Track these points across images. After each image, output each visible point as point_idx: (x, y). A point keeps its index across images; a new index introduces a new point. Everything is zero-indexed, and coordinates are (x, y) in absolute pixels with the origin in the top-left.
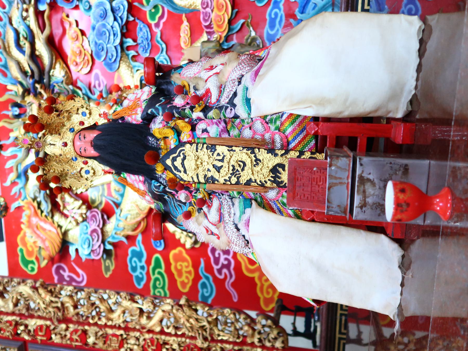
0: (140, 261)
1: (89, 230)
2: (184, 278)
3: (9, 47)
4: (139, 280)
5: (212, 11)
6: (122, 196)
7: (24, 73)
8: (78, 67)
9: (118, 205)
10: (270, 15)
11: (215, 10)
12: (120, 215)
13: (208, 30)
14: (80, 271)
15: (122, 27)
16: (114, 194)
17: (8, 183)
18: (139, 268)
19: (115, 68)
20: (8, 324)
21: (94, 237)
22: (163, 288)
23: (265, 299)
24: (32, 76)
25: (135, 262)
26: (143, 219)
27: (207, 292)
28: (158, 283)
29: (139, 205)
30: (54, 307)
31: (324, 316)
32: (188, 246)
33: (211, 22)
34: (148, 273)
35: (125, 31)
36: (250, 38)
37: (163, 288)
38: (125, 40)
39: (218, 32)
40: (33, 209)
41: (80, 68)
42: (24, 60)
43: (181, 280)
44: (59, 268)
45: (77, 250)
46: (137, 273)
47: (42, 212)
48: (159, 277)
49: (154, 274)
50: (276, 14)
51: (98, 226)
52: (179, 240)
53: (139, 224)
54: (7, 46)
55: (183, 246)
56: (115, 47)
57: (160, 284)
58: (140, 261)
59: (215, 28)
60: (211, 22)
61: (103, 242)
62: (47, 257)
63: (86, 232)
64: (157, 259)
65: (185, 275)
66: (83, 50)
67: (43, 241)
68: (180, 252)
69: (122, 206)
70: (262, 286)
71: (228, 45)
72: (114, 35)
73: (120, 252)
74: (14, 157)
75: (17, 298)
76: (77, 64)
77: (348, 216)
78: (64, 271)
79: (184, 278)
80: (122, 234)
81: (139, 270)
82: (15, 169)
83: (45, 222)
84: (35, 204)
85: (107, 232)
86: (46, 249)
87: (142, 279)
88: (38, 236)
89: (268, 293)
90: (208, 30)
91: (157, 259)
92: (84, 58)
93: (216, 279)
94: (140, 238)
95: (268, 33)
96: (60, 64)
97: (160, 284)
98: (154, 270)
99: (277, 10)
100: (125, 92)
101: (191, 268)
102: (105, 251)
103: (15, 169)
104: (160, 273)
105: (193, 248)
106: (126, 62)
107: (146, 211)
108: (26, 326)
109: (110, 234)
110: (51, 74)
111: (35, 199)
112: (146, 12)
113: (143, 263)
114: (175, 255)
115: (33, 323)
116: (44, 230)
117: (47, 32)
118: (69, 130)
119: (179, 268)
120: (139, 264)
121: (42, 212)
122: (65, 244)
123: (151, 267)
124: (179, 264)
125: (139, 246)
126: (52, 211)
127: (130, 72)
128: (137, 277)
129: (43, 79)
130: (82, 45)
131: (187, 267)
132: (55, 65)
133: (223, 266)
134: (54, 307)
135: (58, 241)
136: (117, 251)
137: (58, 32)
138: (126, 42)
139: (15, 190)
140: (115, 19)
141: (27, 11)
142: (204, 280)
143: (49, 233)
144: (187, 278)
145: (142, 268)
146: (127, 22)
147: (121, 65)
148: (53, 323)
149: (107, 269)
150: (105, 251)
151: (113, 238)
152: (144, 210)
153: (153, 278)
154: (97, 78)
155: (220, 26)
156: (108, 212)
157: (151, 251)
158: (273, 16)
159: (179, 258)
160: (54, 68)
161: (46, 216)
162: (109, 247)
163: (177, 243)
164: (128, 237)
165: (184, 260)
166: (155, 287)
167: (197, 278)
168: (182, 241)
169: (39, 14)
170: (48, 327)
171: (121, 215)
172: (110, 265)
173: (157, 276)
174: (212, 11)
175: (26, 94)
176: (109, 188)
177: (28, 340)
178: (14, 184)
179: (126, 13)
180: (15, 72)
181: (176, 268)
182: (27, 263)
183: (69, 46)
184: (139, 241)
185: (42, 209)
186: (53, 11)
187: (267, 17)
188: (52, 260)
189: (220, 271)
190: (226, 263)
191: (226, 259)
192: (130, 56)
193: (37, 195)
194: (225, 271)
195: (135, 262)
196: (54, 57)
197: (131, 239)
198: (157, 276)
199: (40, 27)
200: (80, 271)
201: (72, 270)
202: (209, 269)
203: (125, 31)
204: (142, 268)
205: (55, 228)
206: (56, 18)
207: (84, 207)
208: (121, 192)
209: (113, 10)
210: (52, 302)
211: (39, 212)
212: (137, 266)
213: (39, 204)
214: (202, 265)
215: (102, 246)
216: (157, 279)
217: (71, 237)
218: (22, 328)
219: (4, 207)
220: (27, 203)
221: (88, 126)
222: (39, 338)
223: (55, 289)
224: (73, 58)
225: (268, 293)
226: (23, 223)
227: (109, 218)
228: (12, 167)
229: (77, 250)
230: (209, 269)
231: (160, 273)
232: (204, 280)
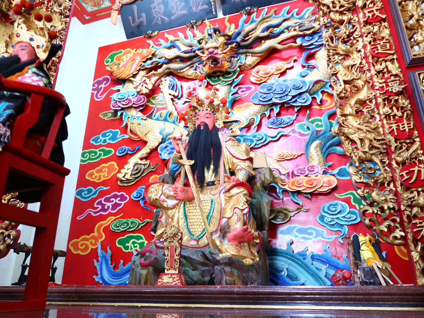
0: (109, 139)
1: (131, 97)
2: (96, 174)
3: (267, 21)
4: (96, 140)
5: (306, 176)
6: (157, 119)
7: (247, 35)
8: (255, 74)
9: (150, 116)
10: (310, 228)
11: (307, 178)
12: (142, 119)
13: (290, 174)
14: (104, 96)
15: (289, 103)
16: (159, 113)
18: (105, 138)
19: (255, 101)
21: (125, 101)
22: (90, 159)
23: (77, 243)
24: (243, 40)
25: (109, 135)
26: (139, 138)
27: (85, 194)
28: (94, 154)
29: (149, 133)
31: (17, 289)
32: (120, 176)
33: (298, 176)
34: (101, 146)
35: (286, 106)
36: (288, 212)
37: (90, 159)
38: (279, 106)
39: (289, 182)
41: (255, 75)
42: (258, 33)
43: (95, 173)
44: (107, 80)
45: (119, 91)
46: (101, 138)
48: (98, 155)
49: (99, 151)
50: (311, 234)
51: (134, 104)
52: (123, 168)
53: (136, 135)
54: (267, 20)
55: (119, 172)
56: (271, 99)
57: (92, 156)
58: (109, 139)
59: (292, 180)
60: (298, 176)
61: (123, 109)
62: (112, 70)
63: (130, 95)
64: (111, 152)
65: (98, 175)
66: (269, 75)
67: (124, 66)
68: (115, 169)
69: (149, 120)
70: (87, 240)
71: (279, 192)
72: (281, 97)
73: (117, 123)
74: (186, 37)
76: (258, 72)
77: (48, 299)
78: (105, 84)
79: (96, 174)
80: (129, 123)
81: (103, 139)
82: (177, 38)
83: (137, 65)
85: (130, 111)
86: (118, 68)
87: (97, 142)
88: (127, 62)
89: (82, 245)
90: (290, 174)
91: (111, 152)
92: (262, 77)
93: (94, 200)
94: (127, 136)
95: (295, 227)
96: (256, 60)
97: (92, 156)
98: (103, 150)
99: (315, 234)
100: (223, 109)
101: (103, 179)
102: (116, 111)
104: (100, 155)
105: (118, 179)
106: (261, 110)
107: (145, 139)
109: (128, 113)
110: (248, 54)
112: (303, 121)
113: (108, 141)
114: (113, 165)
116: (132, 65)
117: (279, 47)
118: (32, 37)
119: (104, 170)
120: (107, 138)
122: (122, 81)
123: (105, 148)
124: (106, 169)
125: (120, 137)
126: (146, 69)
127: (252, 113)
128: (99, 138)
129: (243, 49)
130: (273, 74)
131: (104, 176)
132: (255, 56)
133: (103, 205)
135: (124, 76)
136: (117, 121)
137: (285, 54)
138: (276, 108)
139: (162, 41)
140: (294, 97)
141: (295, 30)
142: (94, 191)
143: (129, 69)
144: (96, 177)
145: (105, 141)
146: (293, 107)
147: (258, 106)
149: (105, 115)
150: (116, 111)
151: (125, 116)
152: (145, 137)
153: (97, 150)
154: (248, 89)
155: (293, 184)
156: (145, 110)
157: (115, 146)
158: (309, 231)
159: (111, 168)
160: (252, 56)
162: (119, 113)
163: (121, 167)
164: (126, 126)
165: (109, 173)
166: (90, 153)
167: (95, 185)
168: (122, 171)
169: (294, 38)
171: (142, 120)
172: (106, 116)
173: (99, 153)
174: (306, 176)
175: (227, 37)
176: (163, 109)
178: (167, 40)
179: (300, 104)
180: (248, 27)
181: (104, 167)
182: (112, 58)
183: (274, 66)
184: (124, 136)
186: (298, 50)
187: (308, 226)
188: (111, 73)
189: (100, 203)
190: (106, 208)
191: (108, 207)
192: (266, 112)
194: (100, 207)
195: (109, 135)
196: (261, 55)
197: (125, 130)
198: (99, 153)
199: (283, 41)
200: (104, 96)
201: (106, 89)
202: (102, 194)
203: (286, 106)
204: (105, 141)
205: (133, 72)
206: (294, 52)
207: (147, 91)
208: (160, 118)
209: (300, 94)
211: (145, 60)
212: (107, 137)
214: (105, 188)
215: (120, 108)
216: (96, 153)
217: (127, 85)
219: (151, 36)
221: (36, 52)
223: (52, 71)
224: (262, 69)
225: (82, 245)
226: (136, 51)
227: (141, 111)
228: (179, 36)
229: (119, 91)
230: (102, 194)
231: (100, 155)
232: (94, 191)
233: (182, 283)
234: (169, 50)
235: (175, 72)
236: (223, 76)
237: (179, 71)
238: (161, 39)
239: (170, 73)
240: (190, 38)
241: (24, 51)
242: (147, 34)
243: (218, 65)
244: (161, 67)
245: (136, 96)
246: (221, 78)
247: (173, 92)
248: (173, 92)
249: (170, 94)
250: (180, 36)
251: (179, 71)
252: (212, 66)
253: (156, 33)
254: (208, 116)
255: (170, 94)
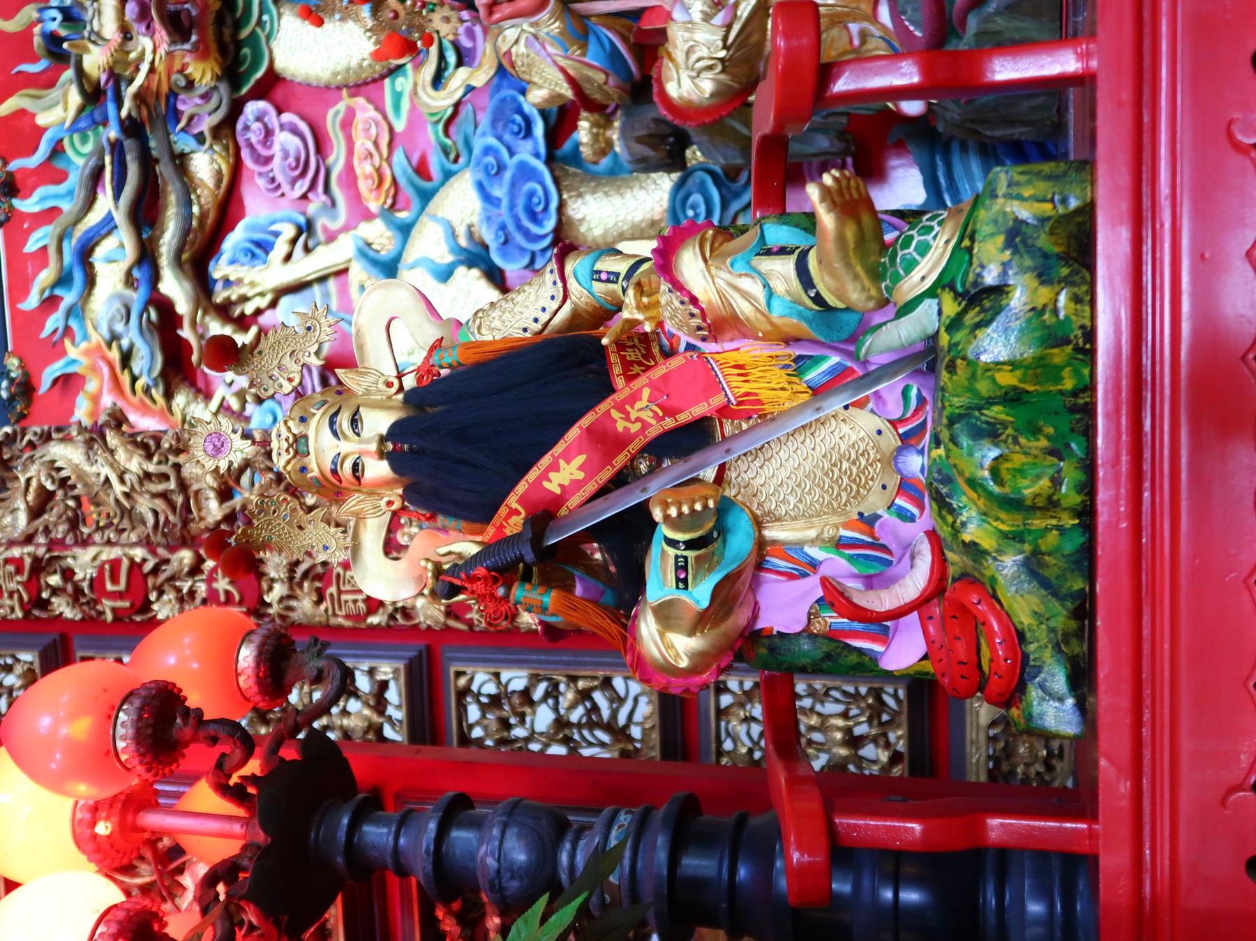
17: (32, 302)
20: (11, 568)
30: (155, 495)
40: (105, 370)
47: (134, 379)
75: (41, 487)
82: (52, 252)
84: (115, 355)
103: (52, 252)
108: (68, 574)
111: (115, 337)
115: (84, 563)
121: (134, 379)
126: (164, 374)
134: (155, 495)
139: (54, 322)
148: (153, 552)
161: (147, 391)
170: (135, 566)
177: (72, 621)
185: (136, 371)
193: (119, 327)
210: (148, 475)
211: (125, 379)
213: (126, 358)
218: (55, 580)
219: (20, 384)
220: (87, 353)
222: (107, 605)
228: (45, 248)
233: (980, 408)
234: (99, 280)
235: (196, 239)
236: (238, 25)
237: (194, 223)
238: (42, 327)
239: (197, 265)
240: (56, 196)
241: (114, 265)
242: (12, 398)
243: (194, 13)
244: (165, 306)
245: (279, 403)
246: (245, 33)
247: (281, 248)
248: (281, 248)
249: (288, 258)
250: (40, 245)
251: (194, 223)
252: (194, 38)
253: (13, 363)
254: (344, 421)
255: (288, 258)
